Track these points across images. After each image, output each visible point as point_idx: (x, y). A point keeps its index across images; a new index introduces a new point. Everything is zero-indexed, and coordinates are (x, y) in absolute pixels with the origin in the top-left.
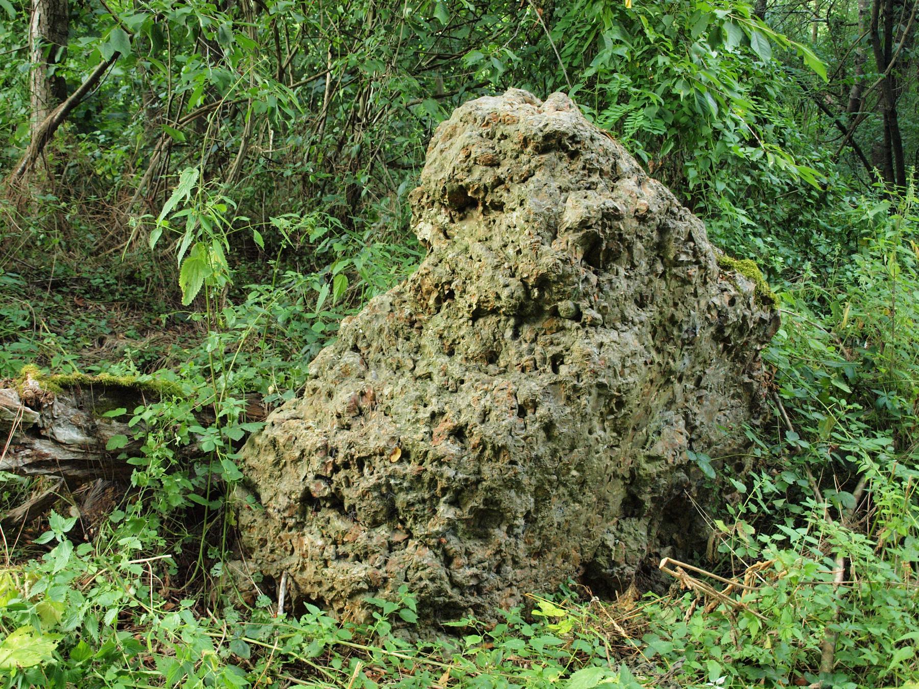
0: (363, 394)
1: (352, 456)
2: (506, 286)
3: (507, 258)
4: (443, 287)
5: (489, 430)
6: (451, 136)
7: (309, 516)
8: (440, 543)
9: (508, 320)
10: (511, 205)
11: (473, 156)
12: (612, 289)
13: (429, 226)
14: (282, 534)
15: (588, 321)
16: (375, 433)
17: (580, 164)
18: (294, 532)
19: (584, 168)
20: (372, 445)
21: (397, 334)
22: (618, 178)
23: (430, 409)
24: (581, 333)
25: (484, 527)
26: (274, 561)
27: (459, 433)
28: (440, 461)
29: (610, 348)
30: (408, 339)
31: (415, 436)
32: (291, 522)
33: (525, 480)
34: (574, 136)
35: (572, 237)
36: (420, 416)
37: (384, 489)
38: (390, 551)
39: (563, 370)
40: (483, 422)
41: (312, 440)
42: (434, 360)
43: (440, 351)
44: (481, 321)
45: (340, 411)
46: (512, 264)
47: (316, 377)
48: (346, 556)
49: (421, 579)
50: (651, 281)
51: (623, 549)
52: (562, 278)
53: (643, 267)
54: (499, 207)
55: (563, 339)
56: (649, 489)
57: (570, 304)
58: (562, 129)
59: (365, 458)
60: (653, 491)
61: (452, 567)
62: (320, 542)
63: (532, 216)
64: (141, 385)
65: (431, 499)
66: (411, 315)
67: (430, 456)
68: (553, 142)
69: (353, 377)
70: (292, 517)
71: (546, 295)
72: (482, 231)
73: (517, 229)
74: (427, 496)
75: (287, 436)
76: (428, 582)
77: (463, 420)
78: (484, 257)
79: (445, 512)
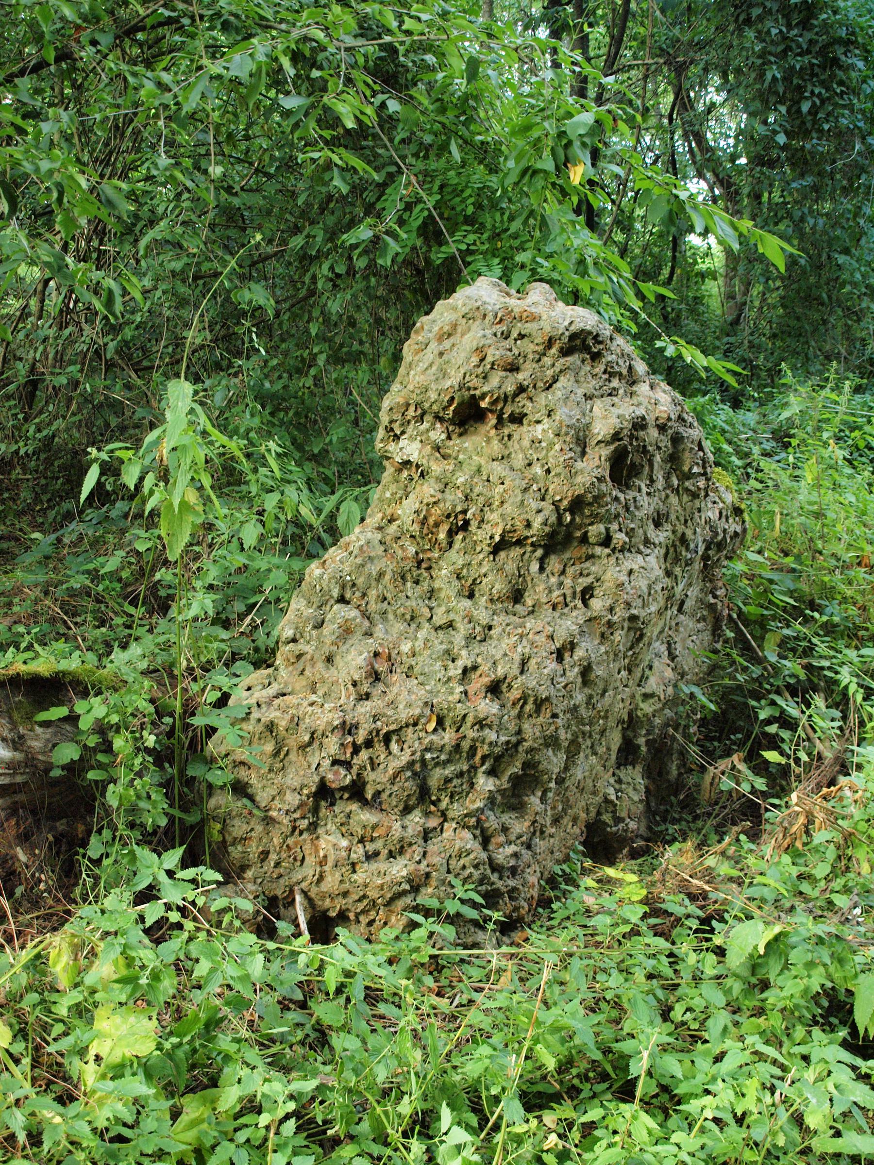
0: (376, 655)
1: (378, 731)
2: (539, 511)
3: (534, 479)
4: (456, 517)
5: (530, 681)
6: (449, 335)
7: (323, 812)
8: (479, 821)
9: (534, 551)
10: (537, 417)
11: (490, 359)
12: (636, 507)
13: (417, 445)
14: (290, 841)
15: (619, 546)
16: (404, 698)
17: (602, 367)
18: (305, 835)
19: (605, 372)
20: (404, 714)
21: (403, 577)
22: (634, 383)
23: (460, 663)
24: (612, 560)
25: (519, 796)
26: (280, 876)
27: (494, 689)
28: (481, 724)
29: (632, 575)
30: (417, 582)
31: (450, 698)
32: (303, 824)
33: (563, 734)
34: (598, 335)
35: (606, 452)
36: (451, 673)
37: (417, 767)
38: (426, 841)
39: (597, 604)
40: (522, 672)
41: (325, 717)
42: (452, 604)
43: (459, 594)
44: (502, 554)
45: (356, 677)
46: (541, 485)
47: (294, 640)
48: (376, 854)
49: (464, 867)
50: (667, 496)
51: (626, 803)
52: (597, 498)
53: (660, 483)
54: (518, 419)
55: (593, 568)
56: (644, 732)
57: (601, 528)
58: (588, 328)
59: (394, 731)
60: (649, 732)
61: (491, 848)
62: (344, 843)
63: (564, 429)
64: (64, 673)
65: (469, 771)
66: (417, 553)
67: (470, 720)
68: (578, 342)
69: (358, 635)
70: (303, 818)
71: (578, 519)
72: (496, 447)
73: (544, 444)
74: (465, 768)
75: (288, 717)
76: (472, 870)
77: (500, 672)
78: (515, 476)
79: (485, 784)
